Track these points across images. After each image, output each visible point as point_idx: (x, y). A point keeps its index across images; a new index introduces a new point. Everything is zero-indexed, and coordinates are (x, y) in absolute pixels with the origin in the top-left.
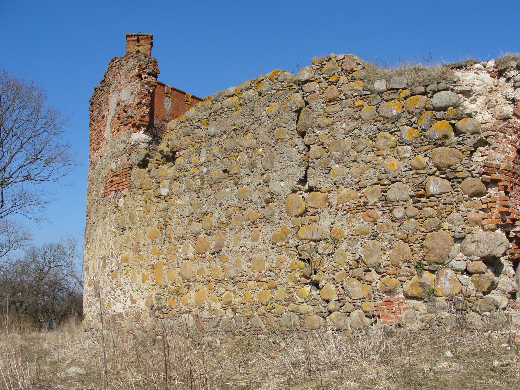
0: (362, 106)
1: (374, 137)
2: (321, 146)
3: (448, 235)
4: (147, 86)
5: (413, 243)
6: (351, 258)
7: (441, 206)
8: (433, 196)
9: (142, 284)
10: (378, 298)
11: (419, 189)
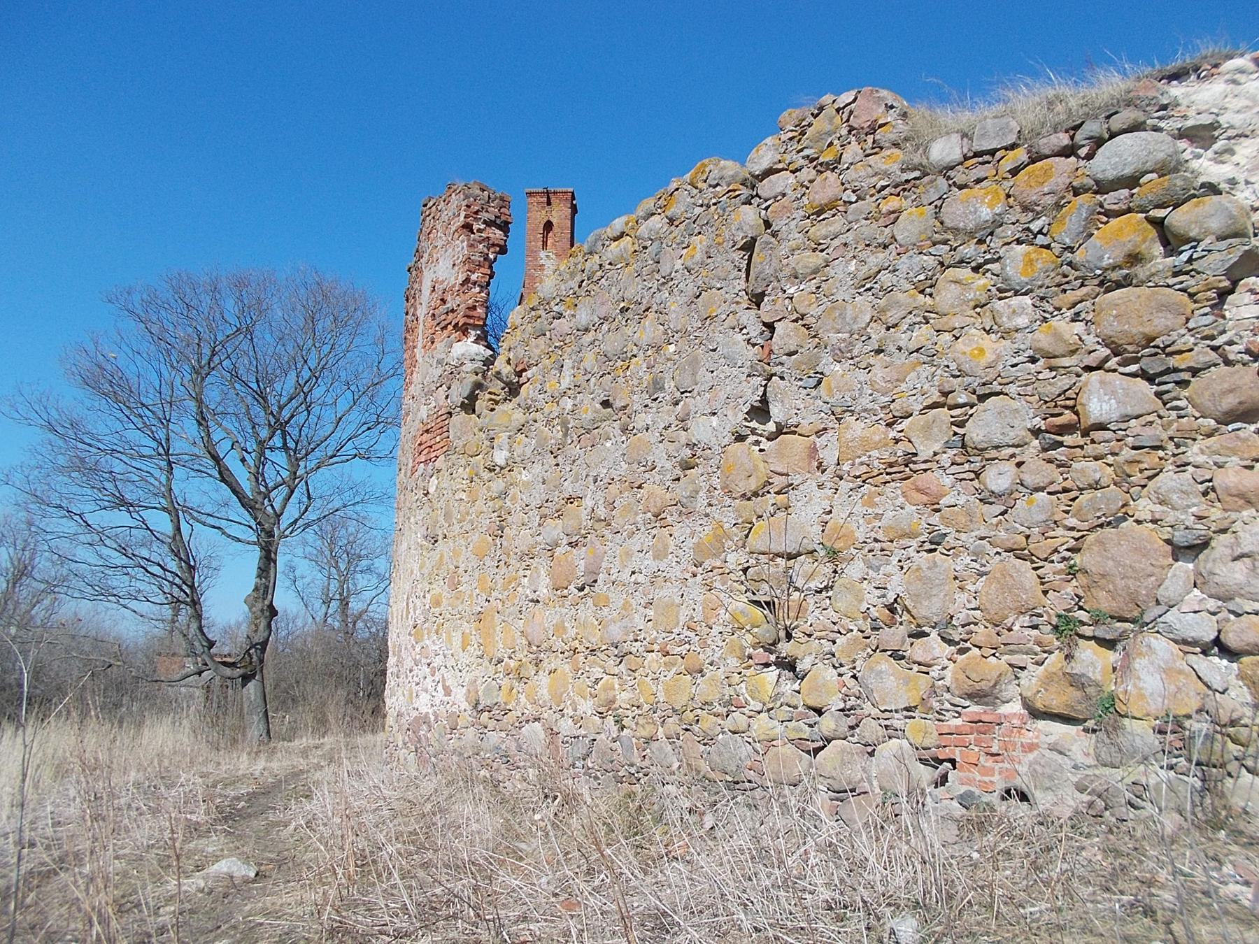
0: (896, 213)
1: (926, 287)
2: (800, 322)
3: (1154, 538)
4: (481, 246)
5: (1046, 560)
6: (874, 601)
7: (1127, 453)
8: (1102, 427)
9: (461, 654)
10: (948, 711)
11: (1057, 411)
